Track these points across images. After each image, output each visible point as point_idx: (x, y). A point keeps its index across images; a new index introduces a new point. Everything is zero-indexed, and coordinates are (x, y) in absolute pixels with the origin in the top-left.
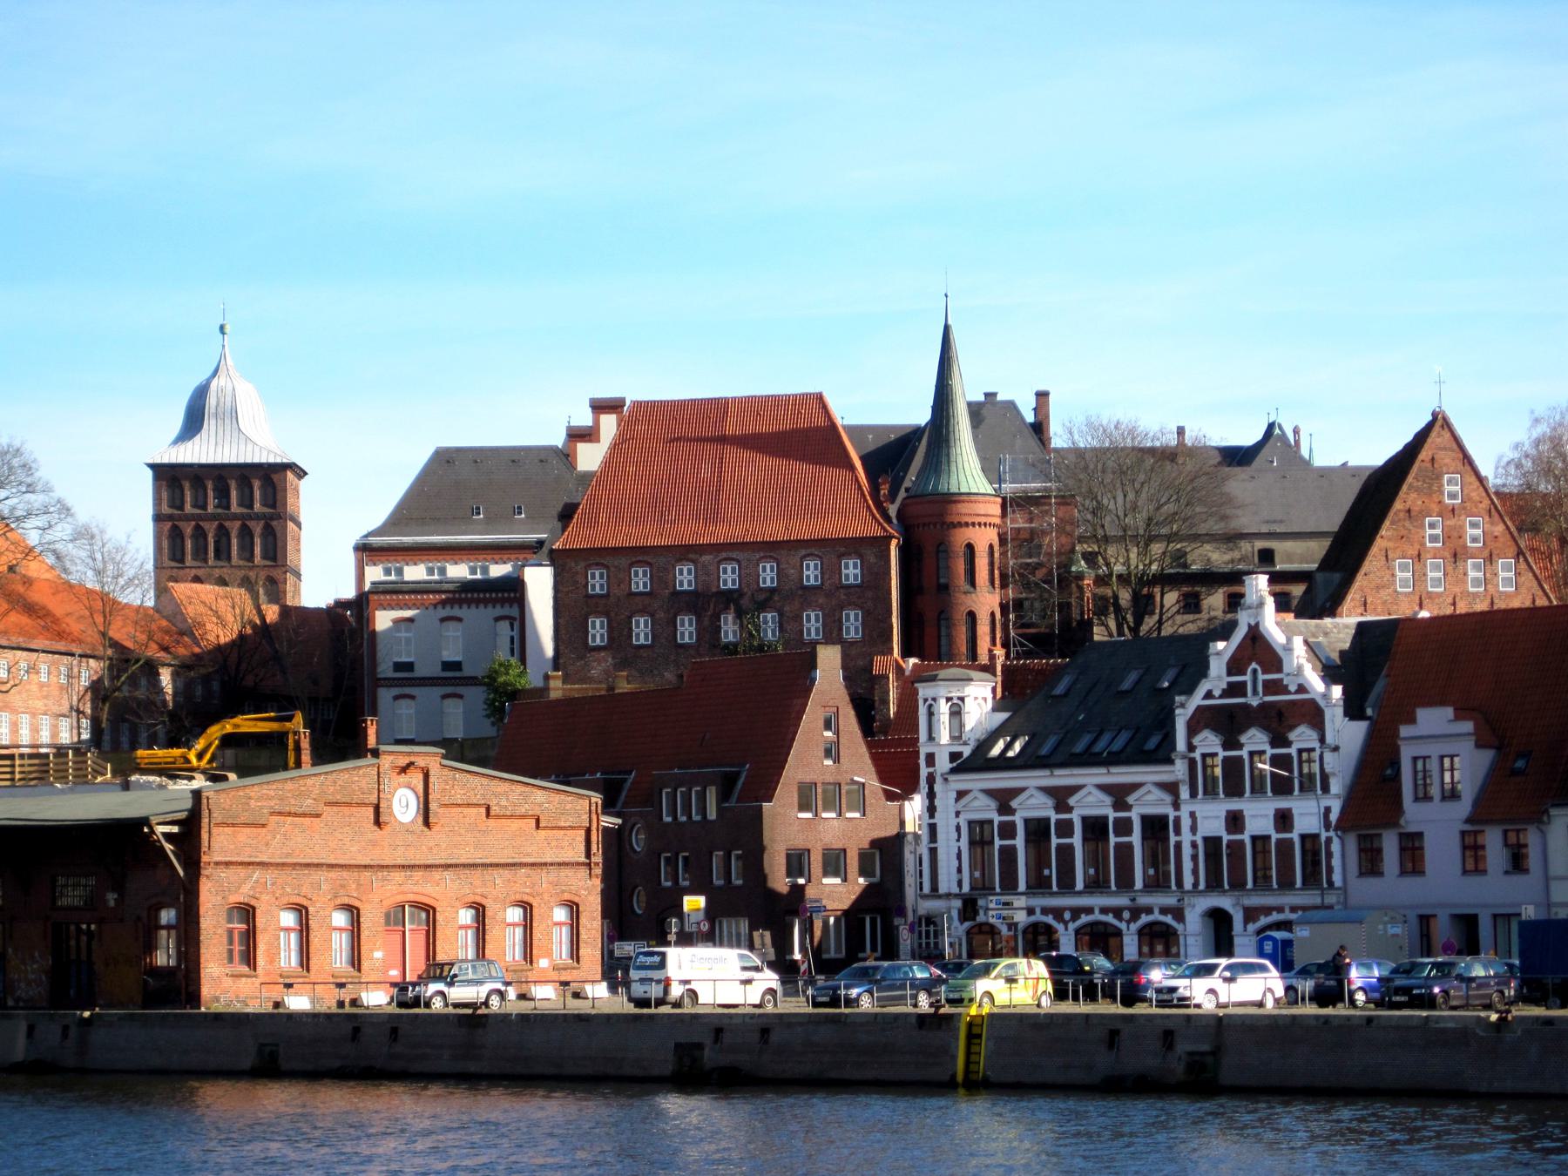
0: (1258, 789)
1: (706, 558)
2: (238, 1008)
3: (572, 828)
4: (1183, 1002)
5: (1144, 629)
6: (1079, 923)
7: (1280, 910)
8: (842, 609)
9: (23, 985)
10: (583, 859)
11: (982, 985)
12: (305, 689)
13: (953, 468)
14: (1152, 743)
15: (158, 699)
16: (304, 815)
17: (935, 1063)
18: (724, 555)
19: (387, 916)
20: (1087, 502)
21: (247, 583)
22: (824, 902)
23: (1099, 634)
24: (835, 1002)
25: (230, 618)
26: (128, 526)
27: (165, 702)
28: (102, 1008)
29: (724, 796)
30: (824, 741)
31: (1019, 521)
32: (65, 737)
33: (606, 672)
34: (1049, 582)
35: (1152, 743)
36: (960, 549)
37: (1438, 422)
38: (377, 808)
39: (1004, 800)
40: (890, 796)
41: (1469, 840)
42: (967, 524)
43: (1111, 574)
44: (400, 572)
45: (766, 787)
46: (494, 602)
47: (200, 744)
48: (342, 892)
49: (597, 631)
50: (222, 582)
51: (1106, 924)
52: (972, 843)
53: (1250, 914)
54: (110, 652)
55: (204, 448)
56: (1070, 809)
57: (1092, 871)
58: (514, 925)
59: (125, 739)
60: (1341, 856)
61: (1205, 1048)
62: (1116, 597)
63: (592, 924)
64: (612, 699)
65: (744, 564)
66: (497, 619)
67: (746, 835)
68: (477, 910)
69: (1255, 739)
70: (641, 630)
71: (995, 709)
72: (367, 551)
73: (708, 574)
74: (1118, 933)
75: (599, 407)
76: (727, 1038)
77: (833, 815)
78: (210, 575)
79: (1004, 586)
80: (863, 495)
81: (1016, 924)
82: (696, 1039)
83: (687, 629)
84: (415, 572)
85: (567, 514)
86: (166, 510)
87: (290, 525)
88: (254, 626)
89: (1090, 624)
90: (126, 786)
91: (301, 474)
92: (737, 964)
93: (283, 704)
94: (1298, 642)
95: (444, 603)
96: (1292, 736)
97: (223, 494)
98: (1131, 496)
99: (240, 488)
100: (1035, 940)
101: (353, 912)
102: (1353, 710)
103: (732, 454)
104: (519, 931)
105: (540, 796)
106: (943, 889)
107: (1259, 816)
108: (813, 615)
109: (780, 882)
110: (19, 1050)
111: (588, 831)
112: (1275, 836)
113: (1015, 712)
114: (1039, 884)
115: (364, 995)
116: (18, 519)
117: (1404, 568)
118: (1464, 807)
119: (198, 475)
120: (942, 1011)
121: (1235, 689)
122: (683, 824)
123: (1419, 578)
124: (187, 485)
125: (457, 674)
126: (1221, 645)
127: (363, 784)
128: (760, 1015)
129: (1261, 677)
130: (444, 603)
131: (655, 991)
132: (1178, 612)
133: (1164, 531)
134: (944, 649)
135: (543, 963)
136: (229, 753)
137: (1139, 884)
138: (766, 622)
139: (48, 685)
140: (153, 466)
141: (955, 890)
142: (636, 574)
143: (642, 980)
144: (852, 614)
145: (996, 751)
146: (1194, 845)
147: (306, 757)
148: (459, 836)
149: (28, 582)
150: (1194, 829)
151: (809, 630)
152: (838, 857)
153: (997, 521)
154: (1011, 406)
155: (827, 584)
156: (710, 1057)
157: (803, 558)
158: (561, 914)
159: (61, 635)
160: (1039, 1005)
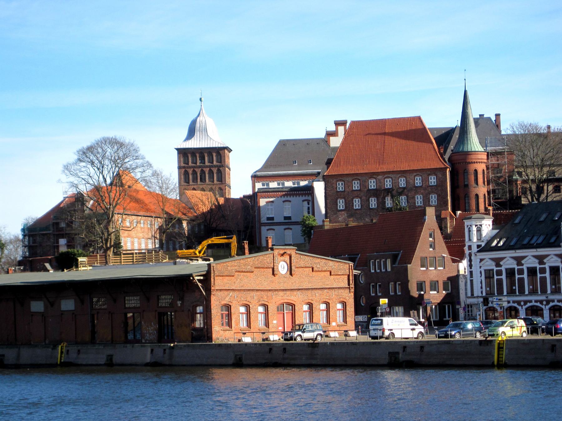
1: (380, 177)
2: (225, 342)
3: (343, 275)
5: (541, 199)
6: (527, 306)
8: (430, 194)
9: (148, 335)
10: (347, 286)
11: (501, 329)
12: (237, 227)
13: (469, 142)
14: (552, 240)
15: (183, 232)
16: (247, 272)
17: (483, 358)
18: (386, 176)
19: (278, 308)
20: (520, 153)
21: (211, 190)
22: (431, 300)
23: (524, 201)
24: (446, 336)
25: (207, 203)
26: (169, 169)
27: (185, 233)
28: (177, 342)
29: (393, 262)
30: (429, 242)
31: (493, 161)
32: (150, 246)
33: (345, 219)
34: (505, 183)
35: (552, 240)
38: (273, 269)
39: (498, 262)
40: (454, 261)
42: (474, 162)
43: (529, 179)
44: (268, 185)
45: (408, 258)
46: (302, 195)
47: (200, 248)
48: (261, 300)
49: (341, 204)
50: (203, 190)
51: (537, 306)
52: (486, 278)
54: (165, 216)
55: (196, 142)
56: (522, 265)
57: (531, 287)
58: (323, 310)
59: (171, 247)
62: (531, 187)
63: (351, 309)
64: (348, 229)
65: (394, 179)
66: (303, 201)
67: (402, 277)
68: (310, 305)
70: (357, 204)
71: (493, 229)
72: (255, 177)
73: (381, 183)
74: (542, 310)
76: (408, 350)
77: (433, 269)
78: (199, 188)
79: (488, 184)
80: (436, 152)
81: (504, 307)
82: (396, 351)
83: (373, 203)
84: (273, 185)
86: (183, 165)
87: (227, 169)
88: (215, 206)
89: (520, 197)
90: (175, 263)
91: (230, 150)
92: (408, 323)
93: (228, 233)
95: (284, 195)
97: (203, 159)
98: (535, 151)
100: (510, 313)
101: (266, 307)
104: (325, 313)
105: (331, 263)
106: (475, 295)
108: (419, 197)
109: (415, 293)
110: (148, 358)
111: (349, 276)
114: (511, 292)
115: (243, 338)
116: (133, 169)
120: (488, 339)
122: (378, 273)
125: (290, 221)
127: (268, 260)
128: (417, 342)
130: (284, 195)
131: (379, 333)
132: (553, 193)
133: (548, 163)
134: (467, 208)
135: (334, 324)
136: (210, 251)
137: (549, 292)
138: (402, 200)
139: (144, 228)
140: (177, 149)
141: (480, 295)
142: (355, 184)
143: (374, 329)
144: (433, 196)
145: (494, 244)
147: (247, 251)
148: (303, 278)
149: (137, 191)
151: (418, 202)
152: (435, 284)
153: (486, 161)
154: (489, 119)
155: (424, 186)
157: (415, 176)
158: (339, 306)
159: (148, 210)
160: (522, 336)
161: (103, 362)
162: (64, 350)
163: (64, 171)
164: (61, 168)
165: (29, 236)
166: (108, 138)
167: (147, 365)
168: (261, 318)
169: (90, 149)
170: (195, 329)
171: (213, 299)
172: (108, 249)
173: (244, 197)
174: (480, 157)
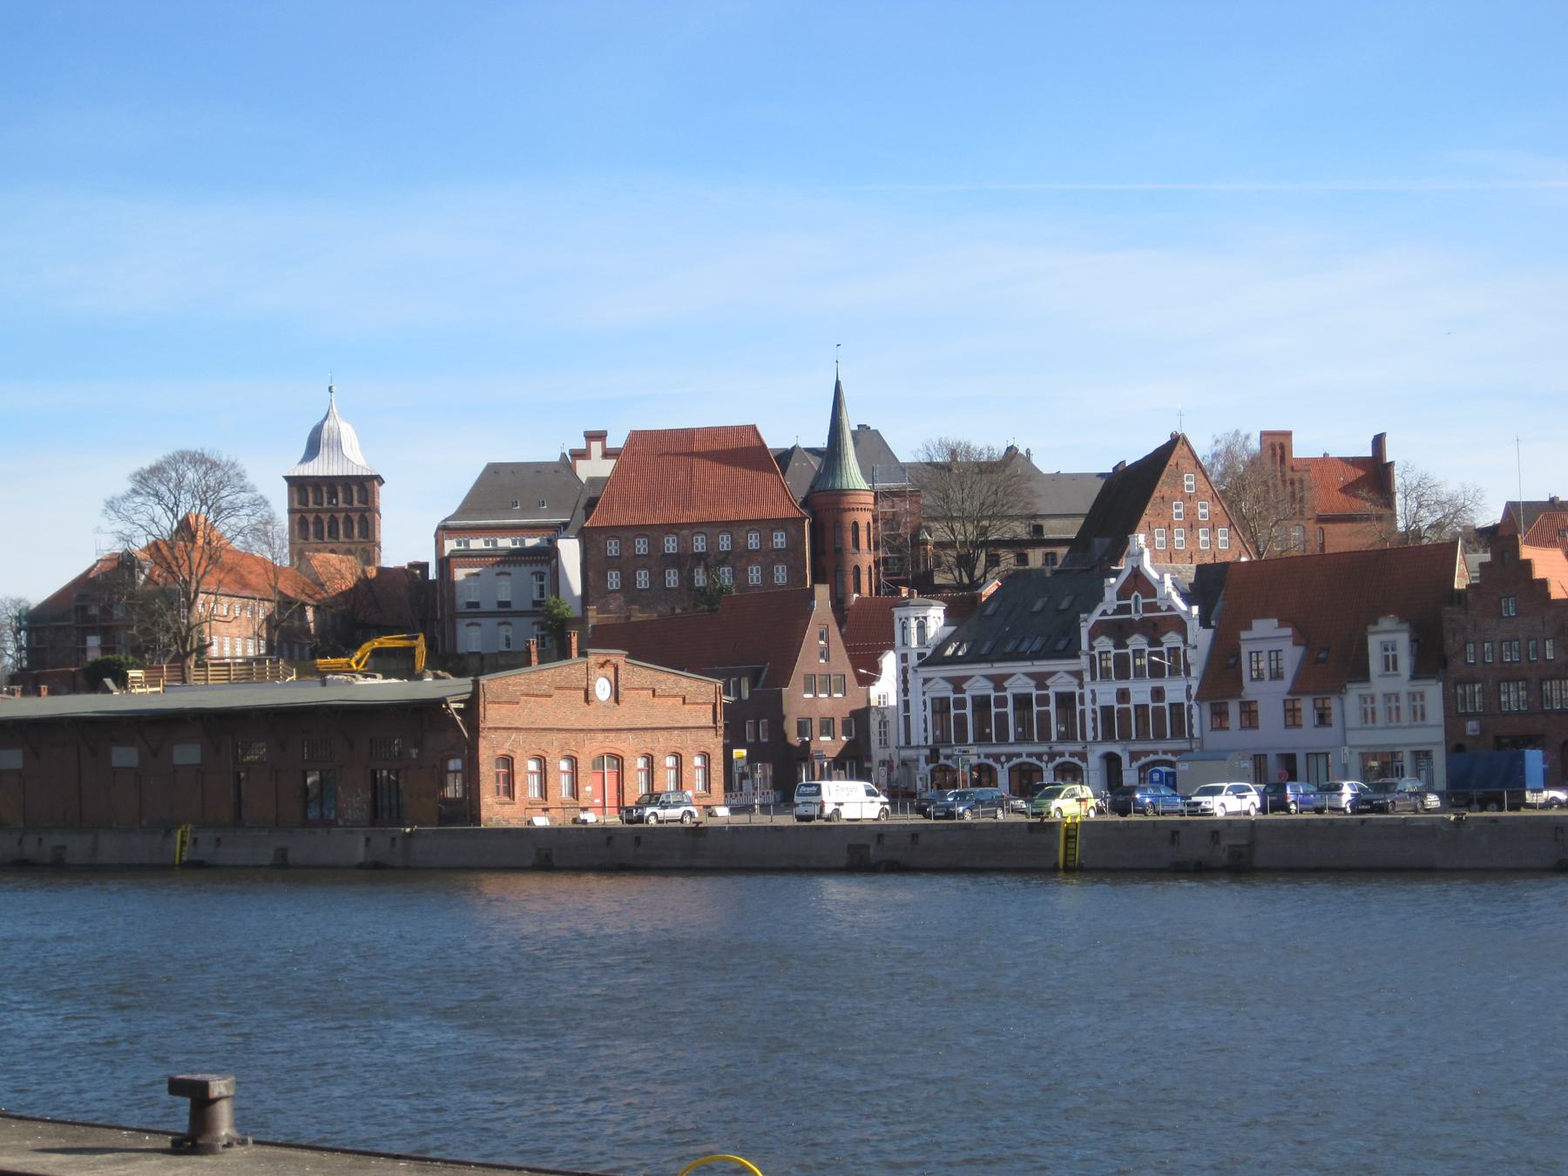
0: (1139, 673)
1: (685, 532)
2: (504, 825)
4: (585, 822)
7: (1155, 752)
11: (1055, 804)
14: (1061, 645)
29: (753, 685)
31: (885, 507)
32: (251, 652)
35: (1061, 645)
36: (849, 526)
37: (1176, 441)
38: (587, 691)
41: (1289, 706)
44: (467, 544)
46: (531, 563)
47: (358, 655)
51: (1030, 764)
52: (934, 712)
53: (1134, 756)
56: (1005, 689)
60: (1198, 717)
61: (1244, 842)
69: (1137, 642)
70: (642, 579)
72: (444, 531)
74: (1040, 770)
75: (591, 436)
79: (876, 548)
83: (672, 579)
84: (477, 544)
85: (591, 504)
86: (297, 506)
91: (382, 482)
94: (1167, 577)
95: (498, 563)
96: (1163, 639)
99: (344, 492)
102: (1204, 621)
103: (699, 464)
104: (673, 773)
105: (685, 682)
107: (1140, 692)
109: (795, 740)
110: (360, 855)
112: (1151, 705)
113: (959, 626)
114: (982, 738)
117: (1160, 534)
118: (1286, 683)
119: (317, 483)
121: (1123, 609)
123: (1170, 540)
124: (310, 490)
126: (1113, 580)
129: (1141, 601)
130: (498, 563)
135: (690, 793)
137: (1054, 738)
145: (949, 652)
146: (1094, 711)
147: (534, 658)
150: (1094, 701)
156: (874, 854)
158: (698, 761)
162: (187, 839)
163: (105, 512)
164: (102, 506)
165: (29, 631)
166: (189, 453)
167: (360, 866)
168: (565, 780)
169: (157, 471)
170: (446, 801)
171: (483, 745)
172: (188, 655)
173: (410, 565)
174: (862, 499)
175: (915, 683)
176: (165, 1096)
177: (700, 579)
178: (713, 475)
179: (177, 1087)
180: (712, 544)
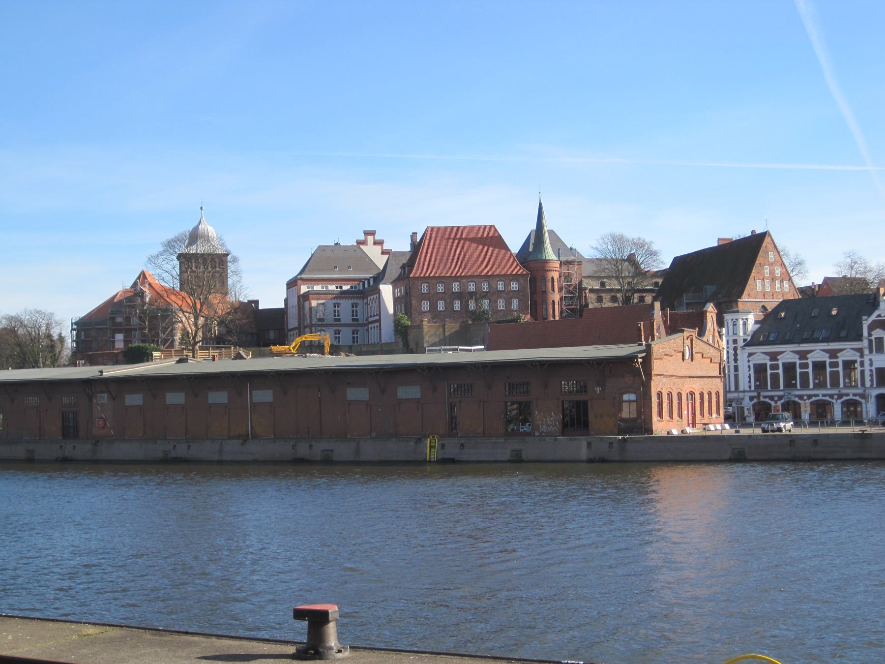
1: (464, 281)
6: (811, 400)
31: (565, 270)
44: (313, 287)
46: (351, 298)
47: (294, 344)
51: (824, 401)
70: (441, 306)
75: (367, 233)
83: (457, 305)
84: (332, 287)
95: (334, 298)
106: (741, 389)
123: (763, 286)
130: (334, 298)
137: (842, 386)
146: (871, 371)
150: (871, 365)
161: (507, 457)
164: (146, 259)
167: (509, 461)
170: (622, 420)
173: (249, 301)
175: (743, 355)
176: (291, 620)
177: (472, 306)
178: (475, 250)
179: (299, 614)
180: (478, 287)
